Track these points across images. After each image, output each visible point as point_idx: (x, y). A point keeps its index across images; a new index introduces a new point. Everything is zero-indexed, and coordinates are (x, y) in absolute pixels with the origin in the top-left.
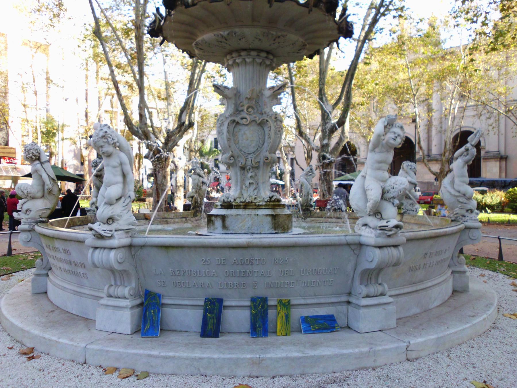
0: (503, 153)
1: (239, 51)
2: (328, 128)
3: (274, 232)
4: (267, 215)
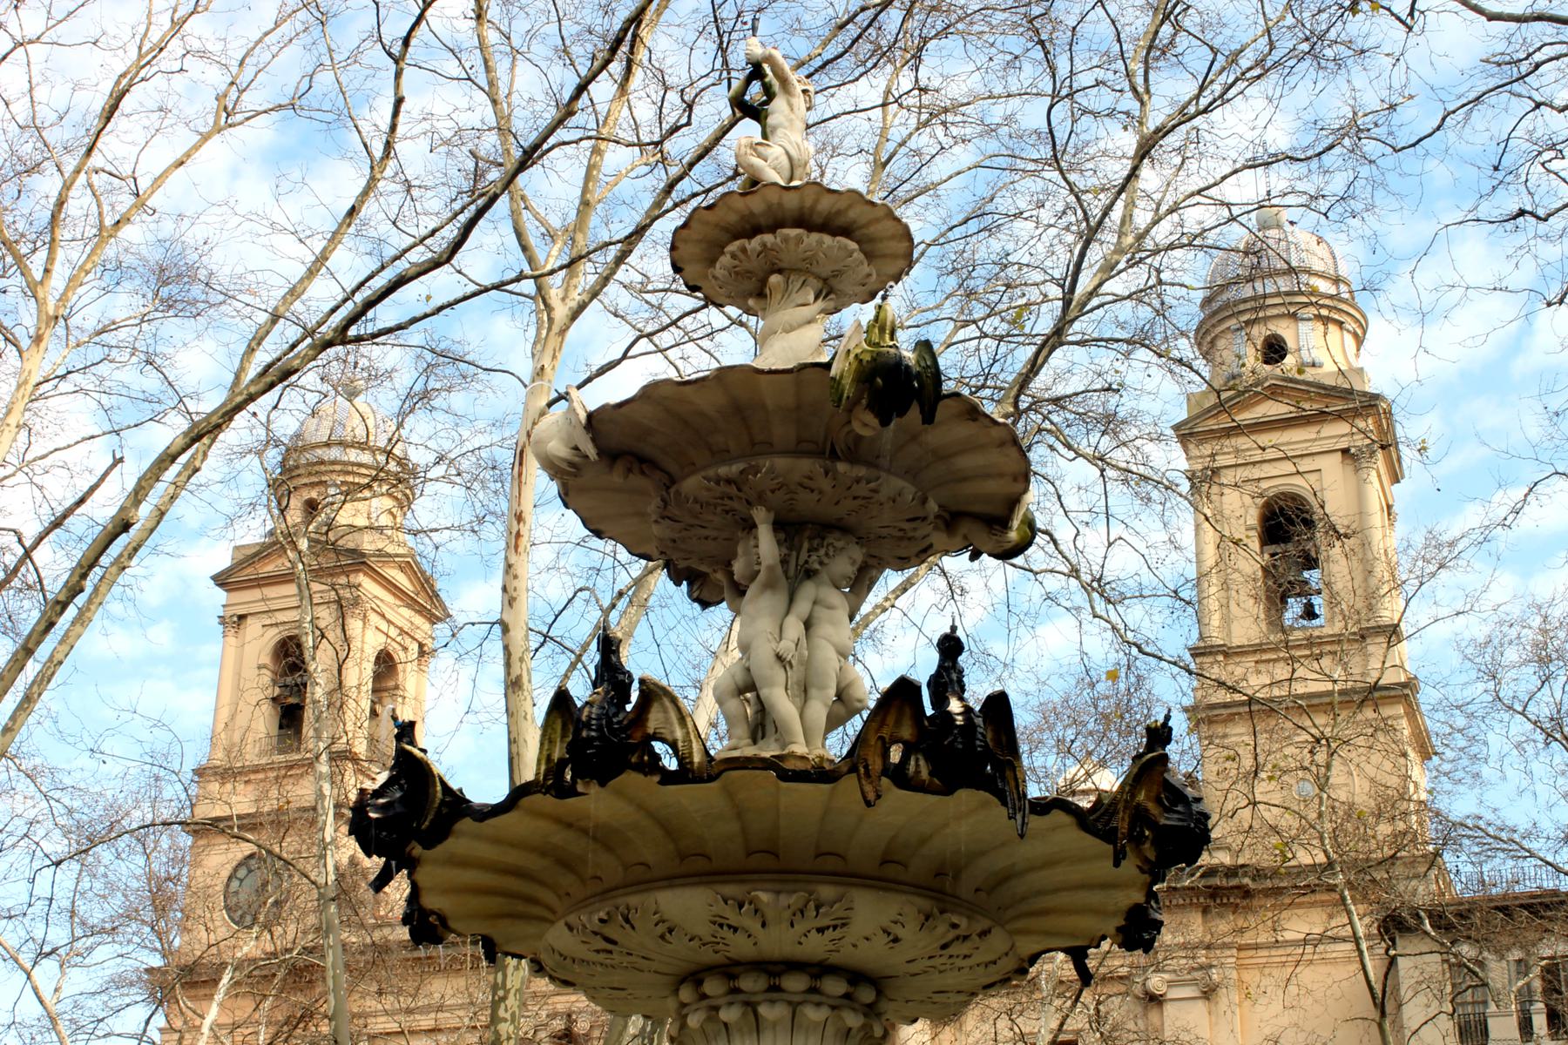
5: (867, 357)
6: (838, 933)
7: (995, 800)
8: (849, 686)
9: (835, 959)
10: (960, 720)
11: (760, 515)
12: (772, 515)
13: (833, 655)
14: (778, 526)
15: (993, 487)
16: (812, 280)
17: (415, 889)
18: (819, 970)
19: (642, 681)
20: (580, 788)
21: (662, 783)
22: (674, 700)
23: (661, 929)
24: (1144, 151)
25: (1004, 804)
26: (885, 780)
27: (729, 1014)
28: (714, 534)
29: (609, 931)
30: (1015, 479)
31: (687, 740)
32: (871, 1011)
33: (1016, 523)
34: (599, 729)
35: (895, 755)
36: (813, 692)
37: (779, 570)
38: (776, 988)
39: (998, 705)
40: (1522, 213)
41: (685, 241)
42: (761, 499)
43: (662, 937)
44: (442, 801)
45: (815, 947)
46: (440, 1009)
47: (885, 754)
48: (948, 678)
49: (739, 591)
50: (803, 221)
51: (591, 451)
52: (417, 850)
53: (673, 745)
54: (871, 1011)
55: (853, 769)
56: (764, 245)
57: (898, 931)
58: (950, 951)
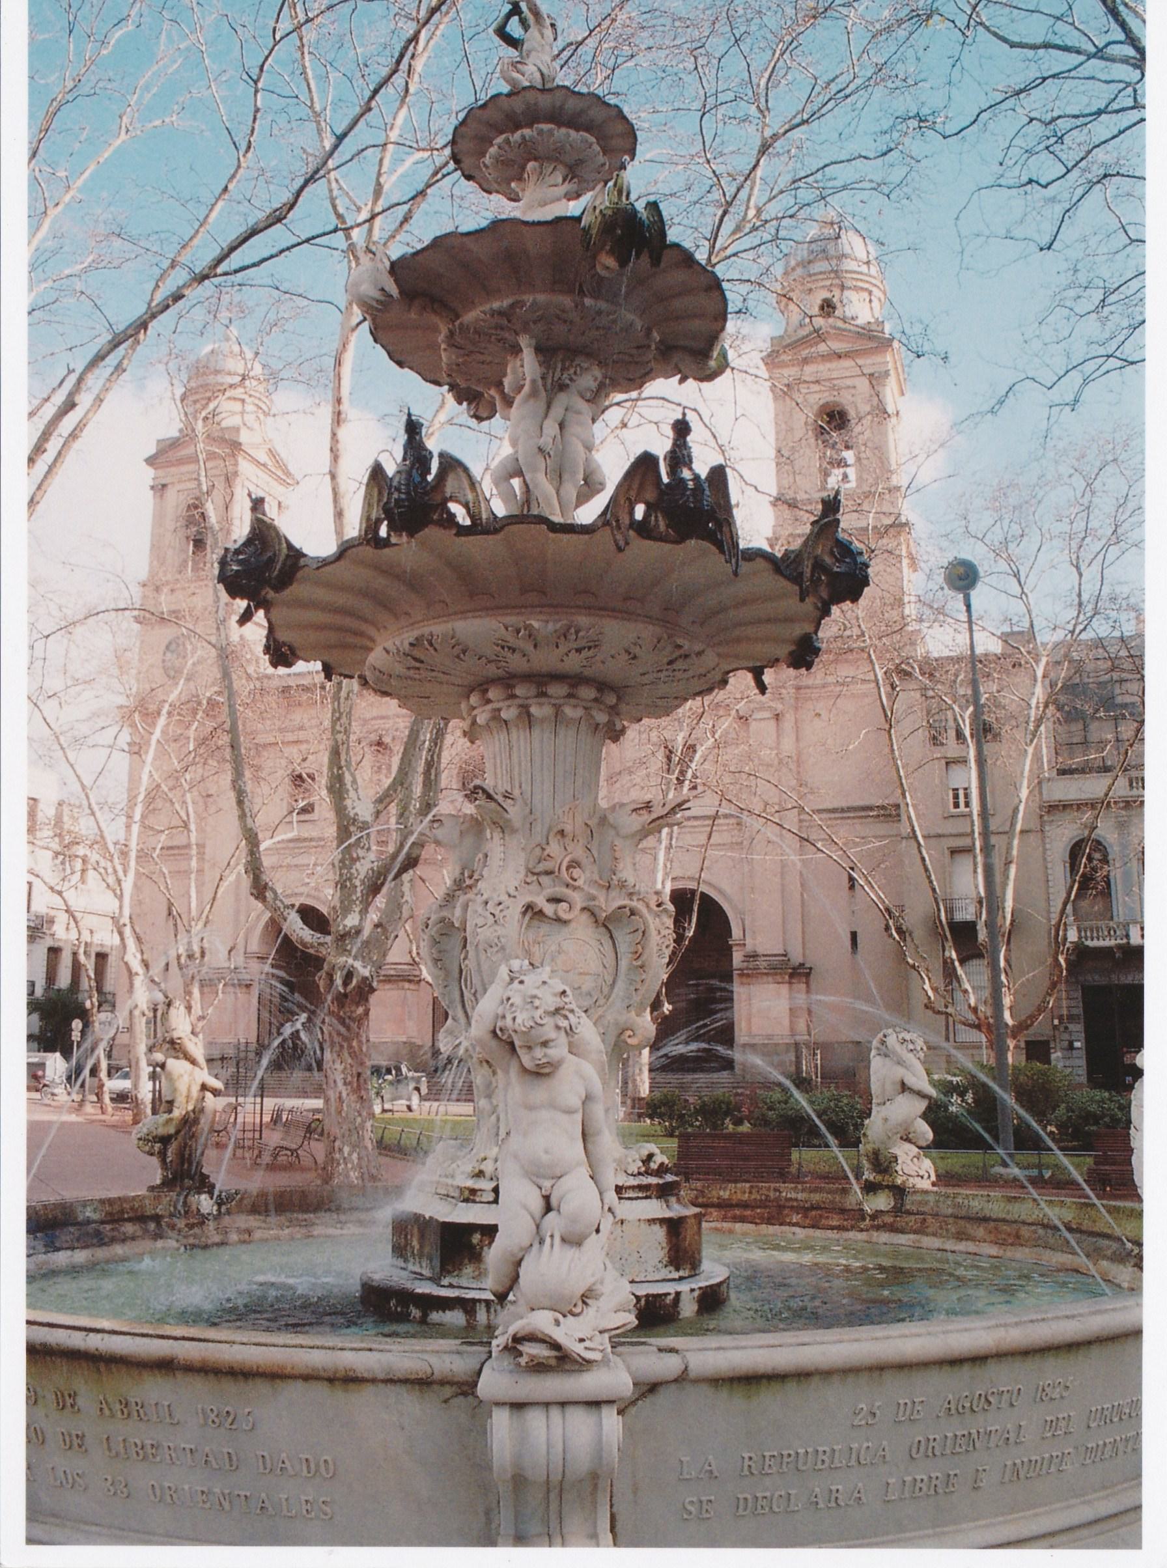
0: (796, 958)
1: (541, 680)
2: (362, 876)
3: (676, 1275)
4: (652, 1221)
5: (609, 212)
6: (591, 653)
7: (713, 548)
8: (592, 473)
9: (587, 672)
10: (691, 485)
11: (524, 341)
12: (533, 342)
13: (581, 448)
14: (539, 350)
15: (696, 325)
16: (560, 167)
17: (271, 630)
18: (575, 681)
19: (441, 455)
20: (394, 540)
21: (458, 534)
22: (466, 470)
23: (457, 650)
24: (764, 148)
25: (722, 552)
26: (631, 533)
27: (508, 714)
28: (489, 359)
29: (417, 653)
30: (716, 319)
31: (477, 501)
32: (614, 710)
33: (715, 354)
34: (408, 493)
35: (640, 511)
36: (565, 477)
37: (540, 382)
38: (543, 694)
39: (718, 475)
40: (1030, 181)
41: (463, 137)
42: (526, 329)
43: (458, 657)
44: (288, 556)
45: (574, 663)
46: (301, 728)
47: (631, 512)
48: (679, 456)
49: (509, 402)
50: (557, 117)
51: (394, 290)
52: (271, 594)
53: (466, 506)
54: (614, 710)
55: (607, 523)
56: (523, 137)
57: (636, 650)
58: (675, 666)
